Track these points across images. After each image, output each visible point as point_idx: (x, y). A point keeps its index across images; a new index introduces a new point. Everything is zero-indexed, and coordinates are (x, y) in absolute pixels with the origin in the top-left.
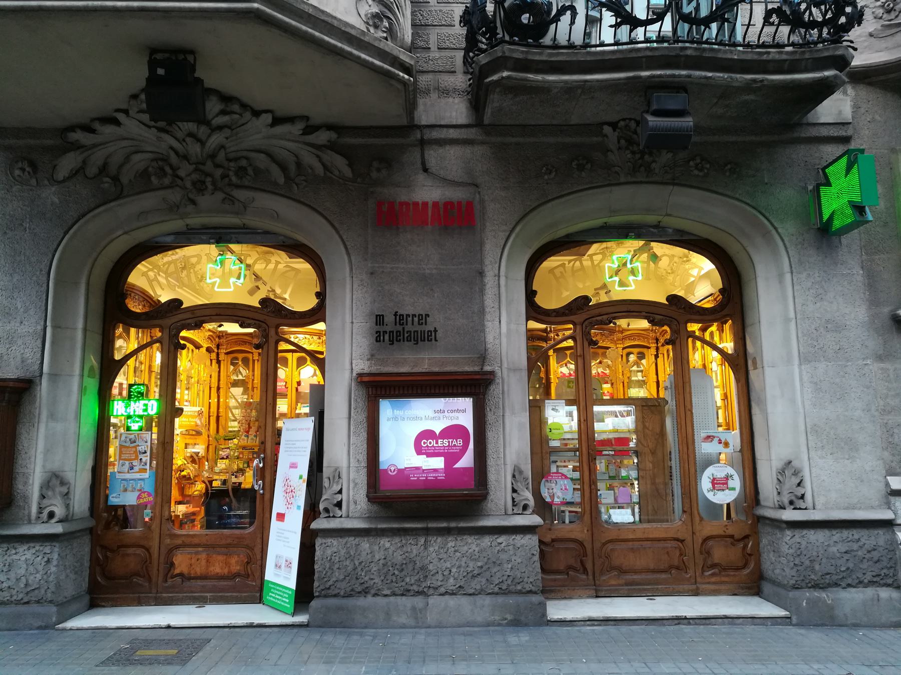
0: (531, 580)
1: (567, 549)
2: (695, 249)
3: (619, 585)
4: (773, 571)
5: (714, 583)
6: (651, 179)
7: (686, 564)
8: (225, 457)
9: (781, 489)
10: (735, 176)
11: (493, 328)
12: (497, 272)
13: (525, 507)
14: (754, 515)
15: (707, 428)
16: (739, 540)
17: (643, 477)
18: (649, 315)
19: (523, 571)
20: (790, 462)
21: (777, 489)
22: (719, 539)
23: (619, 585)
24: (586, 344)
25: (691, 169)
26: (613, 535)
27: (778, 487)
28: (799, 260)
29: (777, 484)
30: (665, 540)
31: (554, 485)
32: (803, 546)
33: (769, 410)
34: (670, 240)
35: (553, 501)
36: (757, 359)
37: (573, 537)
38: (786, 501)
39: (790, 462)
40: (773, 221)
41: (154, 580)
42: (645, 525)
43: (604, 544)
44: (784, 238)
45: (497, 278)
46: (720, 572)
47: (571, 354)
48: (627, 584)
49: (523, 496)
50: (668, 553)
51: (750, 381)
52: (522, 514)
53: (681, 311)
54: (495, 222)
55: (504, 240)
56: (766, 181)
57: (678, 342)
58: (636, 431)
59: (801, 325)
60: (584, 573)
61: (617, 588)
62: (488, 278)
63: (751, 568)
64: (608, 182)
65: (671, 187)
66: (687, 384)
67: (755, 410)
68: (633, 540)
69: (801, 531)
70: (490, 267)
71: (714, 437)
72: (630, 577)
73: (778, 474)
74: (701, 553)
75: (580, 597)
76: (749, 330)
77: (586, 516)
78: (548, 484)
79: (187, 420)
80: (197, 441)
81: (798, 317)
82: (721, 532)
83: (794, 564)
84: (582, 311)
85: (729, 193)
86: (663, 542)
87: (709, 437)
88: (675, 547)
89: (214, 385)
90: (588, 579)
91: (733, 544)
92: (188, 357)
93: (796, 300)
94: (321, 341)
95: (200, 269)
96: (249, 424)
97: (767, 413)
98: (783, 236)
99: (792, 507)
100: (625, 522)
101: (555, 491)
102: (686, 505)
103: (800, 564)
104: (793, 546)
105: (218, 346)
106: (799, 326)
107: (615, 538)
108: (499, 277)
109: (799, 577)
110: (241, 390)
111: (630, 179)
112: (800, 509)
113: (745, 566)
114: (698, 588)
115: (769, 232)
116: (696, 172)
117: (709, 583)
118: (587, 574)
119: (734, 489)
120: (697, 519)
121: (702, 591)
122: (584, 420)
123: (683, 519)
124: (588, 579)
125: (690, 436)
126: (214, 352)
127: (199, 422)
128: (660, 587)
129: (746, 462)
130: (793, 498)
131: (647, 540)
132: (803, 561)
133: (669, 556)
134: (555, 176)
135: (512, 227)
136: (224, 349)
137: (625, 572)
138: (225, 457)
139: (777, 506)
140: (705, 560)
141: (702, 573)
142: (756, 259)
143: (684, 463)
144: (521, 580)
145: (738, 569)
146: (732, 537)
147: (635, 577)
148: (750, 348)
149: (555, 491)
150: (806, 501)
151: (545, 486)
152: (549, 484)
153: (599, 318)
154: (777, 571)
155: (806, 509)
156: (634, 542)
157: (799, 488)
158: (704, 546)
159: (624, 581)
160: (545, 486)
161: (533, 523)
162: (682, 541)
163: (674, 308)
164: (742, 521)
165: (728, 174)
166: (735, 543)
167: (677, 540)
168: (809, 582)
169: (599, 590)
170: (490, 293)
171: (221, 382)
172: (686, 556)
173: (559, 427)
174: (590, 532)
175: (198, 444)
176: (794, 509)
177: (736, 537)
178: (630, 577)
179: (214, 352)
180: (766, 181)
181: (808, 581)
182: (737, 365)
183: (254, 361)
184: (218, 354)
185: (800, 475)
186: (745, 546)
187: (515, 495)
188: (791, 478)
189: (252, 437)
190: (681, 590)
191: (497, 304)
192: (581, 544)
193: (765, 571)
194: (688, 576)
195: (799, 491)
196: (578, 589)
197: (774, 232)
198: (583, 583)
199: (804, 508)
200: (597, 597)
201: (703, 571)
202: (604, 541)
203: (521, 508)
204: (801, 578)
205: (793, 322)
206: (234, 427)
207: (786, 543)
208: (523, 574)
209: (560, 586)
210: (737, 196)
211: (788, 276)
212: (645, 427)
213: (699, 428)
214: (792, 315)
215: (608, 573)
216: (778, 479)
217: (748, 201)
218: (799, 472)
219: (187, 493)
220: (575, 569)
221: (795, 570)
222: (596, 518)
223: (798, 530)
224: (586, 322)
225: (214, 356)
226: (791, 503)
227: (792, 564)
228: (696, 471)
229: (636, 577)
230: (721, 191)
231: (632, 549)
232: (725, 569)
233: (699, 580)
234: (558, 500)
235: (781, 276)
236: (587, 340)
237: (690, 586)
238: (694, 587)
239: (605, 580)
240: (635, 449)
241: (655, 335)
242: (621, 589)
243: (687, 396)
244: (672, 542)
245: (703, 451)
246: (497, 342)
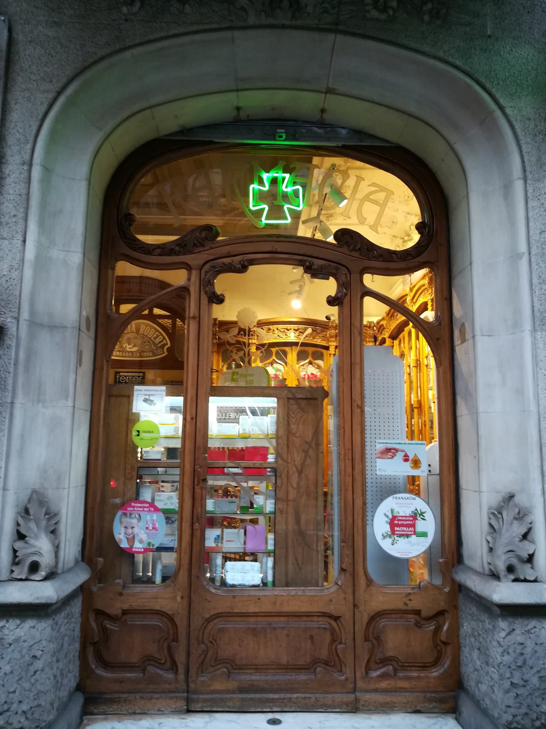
0: (25, 707)
1: (145, 627)
2: (382, 163)
3: (228, 692)
4: (477, 684)
5: (385, 691)
6: (299, 22)
7: (341, 656)
9: (494, 543)
10: (439, 22)
11: (10, 251)
12: (27, 157)
13: (34, 567)
14: (453, 581)
15: (381, 436)
16: (429, 619)
17: (281, 512)
18: (305, 258)
19: (12, 689)
20: (511, 497)
21: (488, 542)
22: (397, 616)
23: (228, 692)
24: (204, 300)
25: (367, 8)
26: (223, 607)
27: (489, 539)
28: (539, 160)
29: (489, 533)
30: (308, 615)
31: (135, 521)
32: (528, 650)
33: (481, 407)
34: (344, 147)
35: (131, 547)
36: (467, 325)
37: (158, 608)
38: (501, 566)
39: (511, 497)
40: (498, 95)
42: (279, 591)
43: (209, 620)
44: (515, 123)
45: (26, 167)
46: (395, 670)
47: (277, 352)
48: (241, 690)
49: (34, 546)
50: (312, 637)
51: (456, 363)
52: (27, 579)
53: (354, 254)
54: (33, 77)
55: (46, 105)
56: (489, 32)
57: (346, 300)
58: (277, 437)
59: (538, 264)
60: (172, 670)
61: (224, 696)
62: (10, 167)
63: (446, 665)
64: (228, 24)
65: (331, 37)
66: (358, 367)
67: (462, 410)
68: (256, 615)
69: (526, 622)
70: (15, 149)
71: (397, 450)
72: (248, 677)
73: (491, 516)
74: (366, 639)
75: (161, 712)
76: (457, 281)
77: (181, 572)
78: (125, 520)
81: (533, 252)
82: (400, 605)
83: (512, 682)
84: (201, 249)
85: (427, 49)
86: (304, 618)
87: (388, 450)
88: (325, 629)
90: (176, 679)
91: (418, 625)
93: (531, 224)
97: (477, 413)
98: (513, 120)
99: (512, 577)
100: (247, 583)
101: (136, 530)
102: (347, 559)
103: (522, 683)
104: (511, 651)
106: (534, 266)
107: (227, 610)
108: (31, 165)
109: (519, 708)
111: (264, 20)
112: (525, 581)
113: (436, 663)
114: (357, 700)
115: (491, 113)
116: (375, 14)
117: (376, 690)
118: (176, 672)
119: (424, 535)
120: (362, 581)
121: (363, 705)
122: (192, 419)
123: (340, 583)
124: (176, 679)
125: (357, 449)
128: (295, 696)
129: (446, 493)
130: (514, 561)
131: (279, 615)
132: (526, 677)
133: (313, 642)
134: (140, 9)
135: (60, 85)
137: (240, 668)
139: (487, 571)
140: (372, 652)
141: (367, 673)
142: (469, 164)
143: (346, 490)
144: (5, 707)
145: (424, 667)
146: (417, 612)
147: (256, 677)
148: (457, 311)
149: (136, 530)
150: (536, 568)
151: (121, 522)
152: (128, 520)
153: (227, 260)
154: (484, 688)
155: (535, 581)
156: (260, 619)
157: (526, 543)
158: (371, 629)
159: (236, 684)
160: (121, 522)
161: (38, 598)
162: (336, 619)
163: (344, 249)
164: (435, 587)
165: (426, 18)
166: (423, 622)
167: (330, 616)
168: (537, 719)
169: (193, 701)
170: (11, 191)
172: (341, 643)
173: (153, 429)
174: (186, 600)
176: (516, 580)
177: (424, 614)
178: (247, 678)
180: (489, 32)
181: (534, 716)
182: (438, 339)
185: (528, 519)
186: (438, 629)
187: (19, 545)
188: (511, 524)
190: (329, 703)
191: (22, 210)
192: (171, 619)
193: (466, 676)
194: (343, 678)
195: (526, 549)
196: (157, 699)
197: (498, 113)
198: (167, 686)
199: (532, 579)
200: (189, 711)
201: (368, 669)
202: (207, 616)
203: (26, 569)
204: (524, 710)
205: (525, 259)
207: (499, 643)
208: (11, 695)
209: (129, 692)
210: (441, 54)
211: (519, 185)
212: (289, 432)
213: (373, 436)
214: (523, 247)
215: (212, 669)
216: (491, 526)
217: (458, 63)
218: (525, 515)
220: (158, 663)
221: (512, 694)
222: (198, 577)
223: (520, 620)
224: (207, 267)
226: (510, 569)
227: (507, 684)
228: (365, 504)
229: (257, 678)
230: (413, 45)
231: (254, 629)
232: (404, 667)
233: (360, 684)
234: (140, 546)
235: (507, 188)
236: (206, 292)
237: (345, 696)
238: (352, 697)
239: (203, 681)
240: (274, 466)
241: (372, 332)
242: (230, 699)
243: (357, 383)
244: (321, 619)
245: (378, 473)
246: (15, 274)
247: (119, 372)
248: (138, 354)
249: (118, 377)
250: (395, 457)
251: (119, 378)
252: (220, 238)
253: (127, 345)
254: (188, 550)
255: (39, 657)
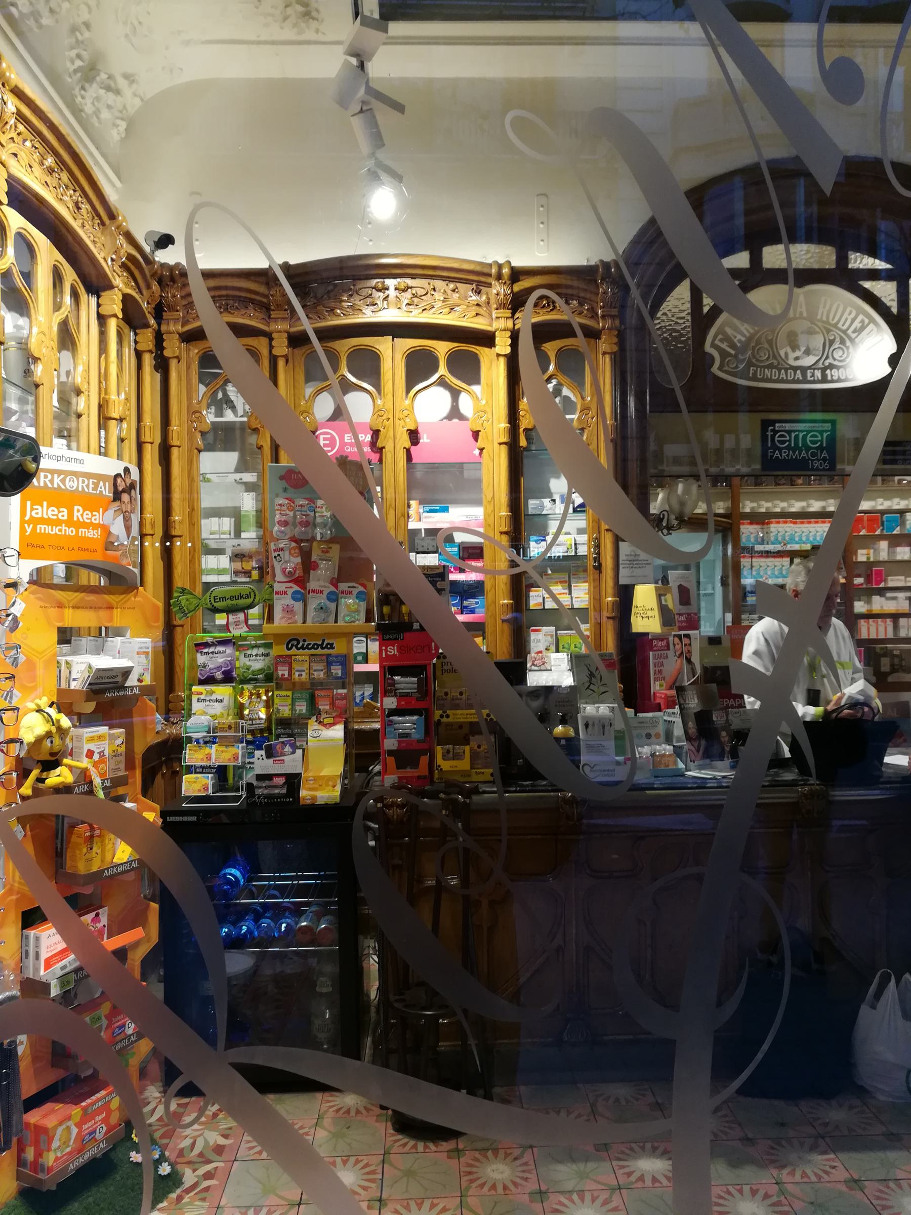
8: (219, 675)
41: (133, 352)
79: (64, 514)
80: (118, 618)
89: (153, 435)
92: (57, 307)
94: (484, 298)
95: (87, 25)
96: (306, 555)
105: (158, 313)
110: (231, 458)
126: (147, 326)
127: (118, 528)
136: (176, 320)
138: (219, 675)
171: (174, 427)
175: (119, 633)
179: (147, 326)
183: (274, 360)
184: (159, 338)
189: (322, 600)
206: (220, 572)
219: (82, 868)
225: (147, 339)
247: (773, 422)
248: (818, 374)
249: (769, 433)
250: (102, 457)
251: (773, 437)
252: (479, 640)
253: (789, 350)
254: (406, 257)
255: (485, 743)
